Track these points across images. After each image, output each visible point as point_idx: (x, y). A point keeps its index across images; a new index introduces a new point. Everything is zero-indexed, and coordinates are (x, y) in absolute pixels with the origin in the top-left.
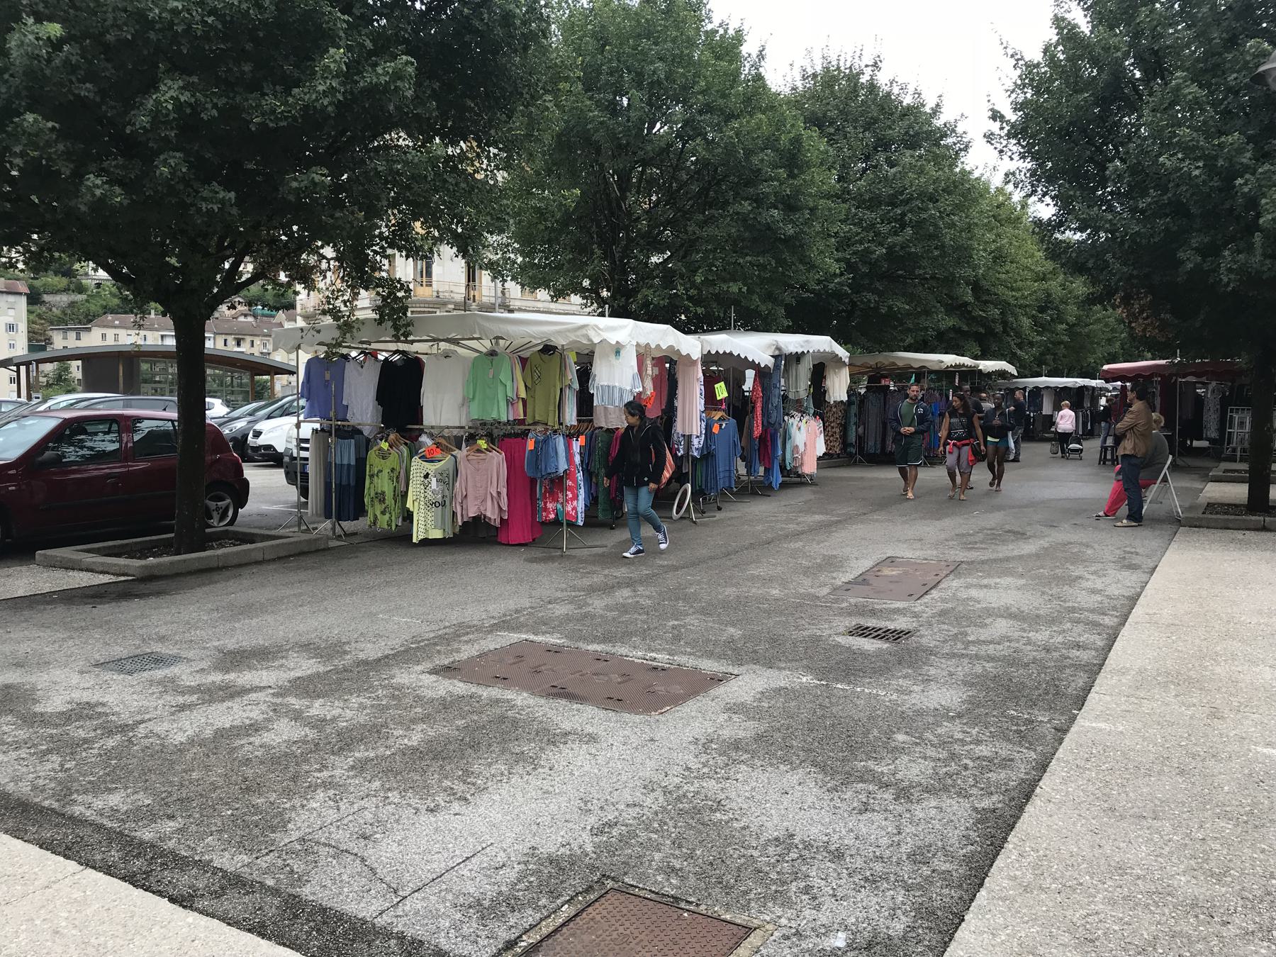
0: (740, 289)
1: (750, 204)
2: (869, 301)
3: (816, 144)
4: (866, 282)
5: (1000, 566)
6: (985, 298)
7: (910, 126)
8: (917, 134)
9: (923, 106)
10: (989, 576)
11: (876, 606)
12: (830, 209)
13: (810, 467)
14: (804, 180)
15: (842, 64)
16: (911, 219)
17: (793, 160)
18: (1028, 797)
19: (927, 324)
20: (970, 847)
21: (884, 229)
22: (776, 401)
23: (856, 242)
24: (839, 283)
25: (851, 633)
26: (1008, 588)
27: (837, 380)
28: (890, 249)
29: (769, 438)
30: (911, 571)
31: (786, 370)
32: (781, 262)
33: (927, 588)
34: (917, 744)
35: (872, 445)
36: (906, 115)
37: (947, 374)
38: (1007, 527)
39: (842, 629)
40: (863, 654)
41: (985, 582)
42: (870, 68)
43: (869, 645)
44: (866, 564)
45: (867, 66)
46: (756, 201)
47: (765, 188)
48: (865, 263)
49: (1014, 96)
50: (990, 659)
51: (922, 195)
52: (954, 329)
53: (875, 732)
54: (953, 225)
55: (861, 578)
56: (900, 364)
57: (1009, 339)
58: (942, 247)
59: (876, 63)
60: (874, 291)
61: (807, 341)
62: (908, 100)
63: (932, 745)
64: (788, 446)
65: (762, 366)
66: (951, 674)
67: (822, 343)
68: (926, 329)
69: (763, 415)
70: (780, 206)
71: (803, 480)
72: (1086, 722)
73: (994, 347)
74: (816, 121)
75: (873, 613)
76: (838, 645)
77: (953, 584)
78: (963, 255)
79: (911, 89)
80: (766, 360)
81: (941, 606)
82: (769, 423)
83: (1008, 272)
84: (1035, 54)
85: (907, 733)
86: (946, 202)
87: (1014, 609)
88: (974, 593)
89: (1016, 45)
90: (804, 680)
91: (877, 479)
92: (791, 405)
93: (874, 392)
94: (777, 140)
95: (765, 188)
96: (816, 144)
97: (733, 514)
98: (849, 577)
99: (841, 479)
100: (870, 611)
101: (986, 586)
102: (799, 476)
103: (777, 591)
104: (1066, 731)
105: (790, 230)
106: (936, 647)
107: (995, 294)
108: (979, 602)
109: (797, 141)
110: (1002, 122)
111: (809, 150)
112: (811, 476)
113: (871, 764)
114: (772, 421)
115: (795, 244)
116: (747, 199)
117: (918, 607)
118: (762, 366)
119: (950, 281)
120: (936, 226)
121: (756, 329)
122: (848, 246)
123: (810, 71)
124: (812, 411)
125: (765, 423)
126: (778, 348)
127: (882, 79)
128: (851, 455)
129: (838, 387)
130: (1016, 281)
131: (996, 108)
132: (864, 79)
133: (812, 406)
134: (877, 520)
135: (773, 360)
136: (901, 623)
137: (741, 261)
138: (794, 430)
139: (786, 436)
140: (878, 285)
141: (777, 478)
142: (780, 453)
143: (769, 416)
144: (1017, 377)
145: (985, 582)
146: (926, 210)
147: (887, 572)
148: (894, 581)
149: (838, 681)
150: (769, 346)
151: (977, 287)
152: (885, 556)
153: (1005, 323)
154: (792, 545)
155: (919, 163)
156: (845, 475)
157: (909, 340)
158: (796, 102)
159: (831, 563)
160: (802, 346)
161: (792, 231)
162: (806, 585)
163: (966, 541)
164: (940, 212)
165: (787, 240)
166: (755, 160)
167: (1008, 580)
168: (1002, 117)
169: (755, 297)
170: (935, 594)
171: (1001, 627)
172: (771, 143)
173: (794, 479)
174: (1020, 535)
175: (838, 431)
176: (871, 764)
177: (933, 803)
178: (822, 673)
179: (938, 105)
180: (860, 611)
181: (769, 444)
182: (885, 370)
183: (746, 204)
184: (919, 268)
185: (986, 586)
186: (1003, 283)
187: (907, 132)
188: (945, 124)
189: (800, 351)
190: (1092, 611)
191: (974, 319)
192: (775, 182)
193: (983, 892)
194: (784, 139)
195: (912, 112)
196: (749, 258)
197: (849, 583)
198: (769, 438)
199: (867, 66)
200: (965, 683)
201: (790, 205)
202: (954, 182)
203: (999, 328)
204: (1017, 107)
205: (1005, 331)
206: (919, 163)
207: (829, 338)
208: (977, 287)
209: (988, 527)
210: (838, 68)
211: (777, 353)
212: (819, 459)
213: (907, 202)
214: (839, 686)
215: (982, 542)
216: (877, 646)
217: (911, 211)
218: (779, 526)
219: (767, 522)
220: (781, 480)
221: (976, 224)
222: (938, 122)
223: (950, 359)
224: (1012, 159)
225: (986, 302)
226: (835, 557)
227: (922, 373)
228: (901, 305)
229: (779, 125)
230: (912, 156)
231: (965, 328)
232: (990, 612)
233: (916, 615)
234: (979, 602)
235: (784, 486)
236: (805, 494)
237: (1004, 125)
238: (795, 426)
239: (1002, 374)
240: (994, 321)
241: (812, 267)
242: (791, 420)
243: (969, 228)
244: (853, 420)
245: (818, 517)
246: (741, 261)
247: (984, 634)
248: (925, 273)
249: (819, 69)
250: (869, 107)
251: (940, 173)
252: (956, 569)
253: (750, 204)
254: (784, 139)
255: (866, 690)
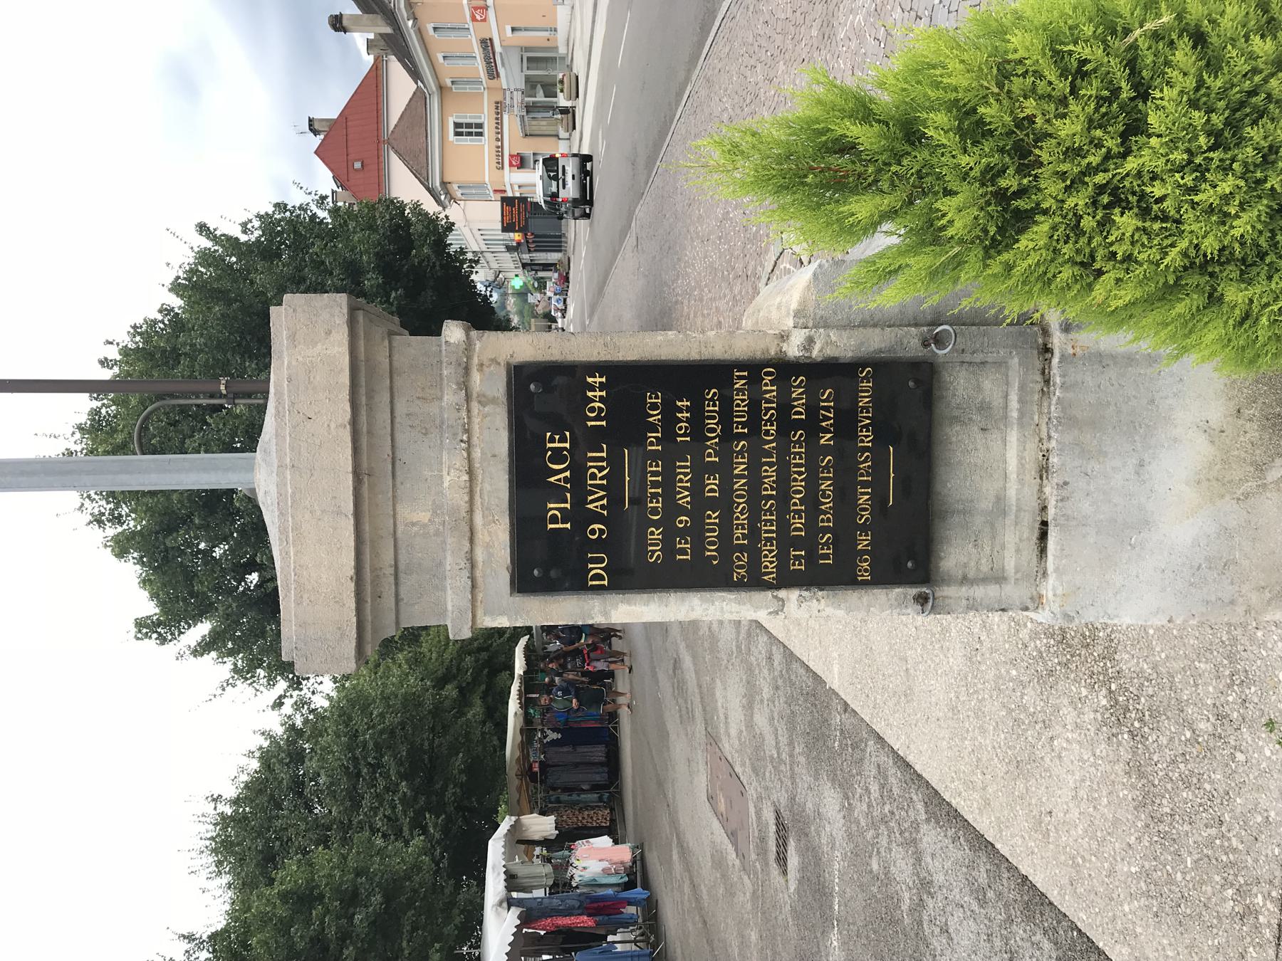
0: (437, 951)
1: (347, 948)
2: (454, 794)
3: (290, 873)
4: (434, 798)
5: (707, 696)
6: (455, 671)
7: (281, 762)
8: (289, 755)
9: (261, 748)
10: (716, 709)
11: (756, 834)
12: (358, 853)
13: (624, 853)
14: (326, 885)
15: (209, 835)
16: (374, 758)
17: (303, 900)
18: (908, 765)
19: (478, 732)
20: (962, 839)
21: (382, 783)
22: (556, 902)
23: (394, 812)
24: (435, 827)
25: (785, 873)
26: (725, 697)
27: (534, 828)
28: (403, 777)
29: (596, 905)
30: (719, 783)
31: (524, 890)
32: (410, 904)
33: (734, 775)
34: (878, 852)
35: (600, 777)
36: (269, 766)
37: (526, 703)
38: (671, 672)
39: (782, 881)
40: (803, 868)
41: (722, 717)
42: (219, 806)
43: (793, 861)
44: (716, 824)
45: (215, 809)
46: (344, 940)
47: (331, 932)
48: (415, 799)
49: (262, 688)
50: (791, 743)
51: (350, 749)
52: (483, 698)
53: (875, 889)
54: (382, 715)
55: (732, 839)
56: (518, 754)
57: (495, 644)
58: (403, 725)
59: (213, 800)
60: (444, 788)
61: (493, 868)
62: (255, 765)
63: (877, 837)
64: (604, 881)
65: (518, 922)
66: (810, 788)
67: (496, 848)
68: (483, 733)
69: (571, 915)
70: (351, 910)
71: (638, 858)
72: (835, 680)
73: (502, 658)
74: (269, 859)
75: (763, 839)
76: (798, 890)
77: (727, 747)
78: (411, 701)
79: (244, 761)
80: (512, 918)
81: (749, 770)
82: (579, 908)
83: (430, 651)
84: (225, 670)
85: (870, 857)
86: (359, 722)
87: (744, 701)
88: (733, 732)
89: (214, 686)
90: (835, 943)
91: (633, 777)
92: (561, 885)
93: (546, 778)
94: (281, 919)
95: (331, 932)
96: (290, 873)
97: (679, 951)
98: (730, 849)
99: (635, 814)
100: (762, 842)
101: (726, 718)
102: (634, 862)
103: (753, 933)
104: (846, 704)
105: (377, 899)
106: (787, 791)
107: (451, 661)
108: (741, 731)
109: (284, 896)
110: (285, 696)
111: (295, 882)
112: (633, 849)
113: (905, 907)
114: (577, 904)
115: (392, 890)
116: (341, 953)
117: (752, 792)
118: (518, 922)
119: (436, 711)
120: (382, 732)
121: (480, 922)
122: (397, 820)
123: (214, 868)
124: (566, 853)
125: (580, 911)
126: (500, 904)
127: (231, 792)
128: (612, 795)
129: (542, 825)
130: (440, 641)
131: (271, 704)
132: (228, 810)
133: (561, 853)
134: (674, 797)
135: (513, 909)
136: (769, 816)
137: (406, 952)
138: (587, 875)
139: (593, 884)
140: (438, 786)
141: (638, 892)
142: (610, 891)
143: (573, 908)
144: (532, 636)
145: (722, 717)
146: (365, 743)
147: (722, 807)
148: (730, 803)
149: (831, 907)
150: (498, 914)
151: (441, 682)
152: (707, 803)
153: (480, 650)
154: (705, 897)
155: (319, 752)
156: (631, 813)
157: (496, 742)
158: (245, 887)
159: (719, 862)
160: (499, 874)
161: (378, 897)
162: (744, 898)
163: (687, 717)
164: (368, 729)
165: (388, 899)
166: (301, 945)
167: (718, 694)
168: (280, 697)
169: (446, 931)
170: (738, 769)
171: (761, 720)
172: (284, 927)
173: (637, 874)
174: (677, 664)
175: (586, 813)
176: (905, 907)
177: (929, 859)
178: (827, 920)
179: (263, 734)
180: (762, 852)
181: (601, 904)
182: (524, 765)
183: (346, 952)
184: (422, 745)
185: (726, 718)
186: (440, 655)
187: (287, 764)
188: (282, 725)
189: (503, 877)
190: (738, 633)
191: (474, 679)
192: (324, 919)
193: (998, 846)
194: (282, 911)
195: (266, 758)
196: (404, 944)
197: (736, 850)
198: (596, 905)
199: (215, 809)
200: (817, 779)
201: (351, 899)
202: (340, 716)
203: (484, 655)
204: (271, 682)
205: (487, 649)
206: (319, 752)
207: (490, 842)
208: (441, 682)
209: (671, 690)
210: (212, 839)
211: (505, 905)
212: (616, 842)
213: (355, 759)
214: (836, 907)
215: (686, 702)
216: (794, 852)
217: (365, 758)
218: (687, 904)
219: (684, 914)
220: (639, 889)
221: (383, 691)
222: (279, 731)
223: (513, 706)
224: (321, 683)
225: (458, 669)
226: (712, 855)
227: (528, 729)
228: (459, 761)
229: (265, 919)
230: (311, 759)
231: (483, 687)
232: (750, 725)
233: (760, 798)
234: (741, 731)
235: (646, 885)
236: (653, 859)
237: (288, 694)
238: (582, 873)
239: (528, 650)
240: (477, 661)
241: (417, 867)
242: (577, 879)
243: (386, 698)
244: (575, 797)
245: (675, 857)
246: (406, 952)
247: (770, 740)
248: (428, 739)
249: (211, 859)
250: (257, 805)
251: (330, 731)
252: (713, 740)
253: (347, 948)
254: (282, 911)
255: (837, 880)
